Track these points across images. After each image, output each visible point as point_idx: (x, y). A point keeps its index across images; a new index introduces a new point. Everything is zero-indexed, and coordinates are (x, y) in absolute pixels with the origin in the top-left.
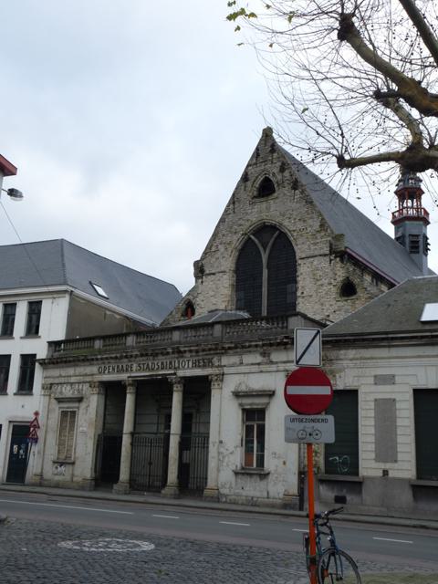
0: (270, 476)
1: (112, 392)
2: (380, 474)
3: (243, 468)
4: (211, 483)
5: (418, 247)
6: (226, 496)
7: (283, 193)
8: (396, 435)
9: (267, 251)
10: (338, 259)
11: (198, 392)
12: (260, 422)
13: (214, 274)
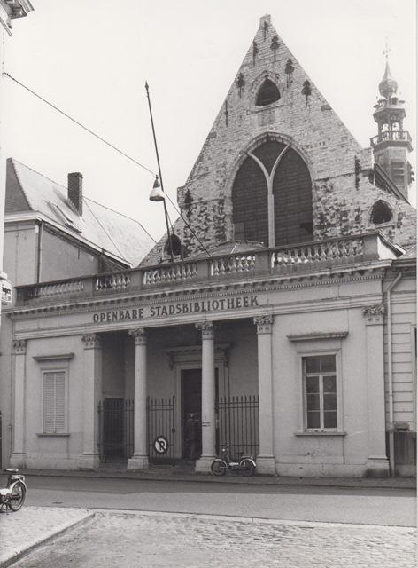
1: (114, 348)
7: (291, 97)
9: (273, 172)
10: (367, 178)
11: (237, 339)
12: (331, 374)
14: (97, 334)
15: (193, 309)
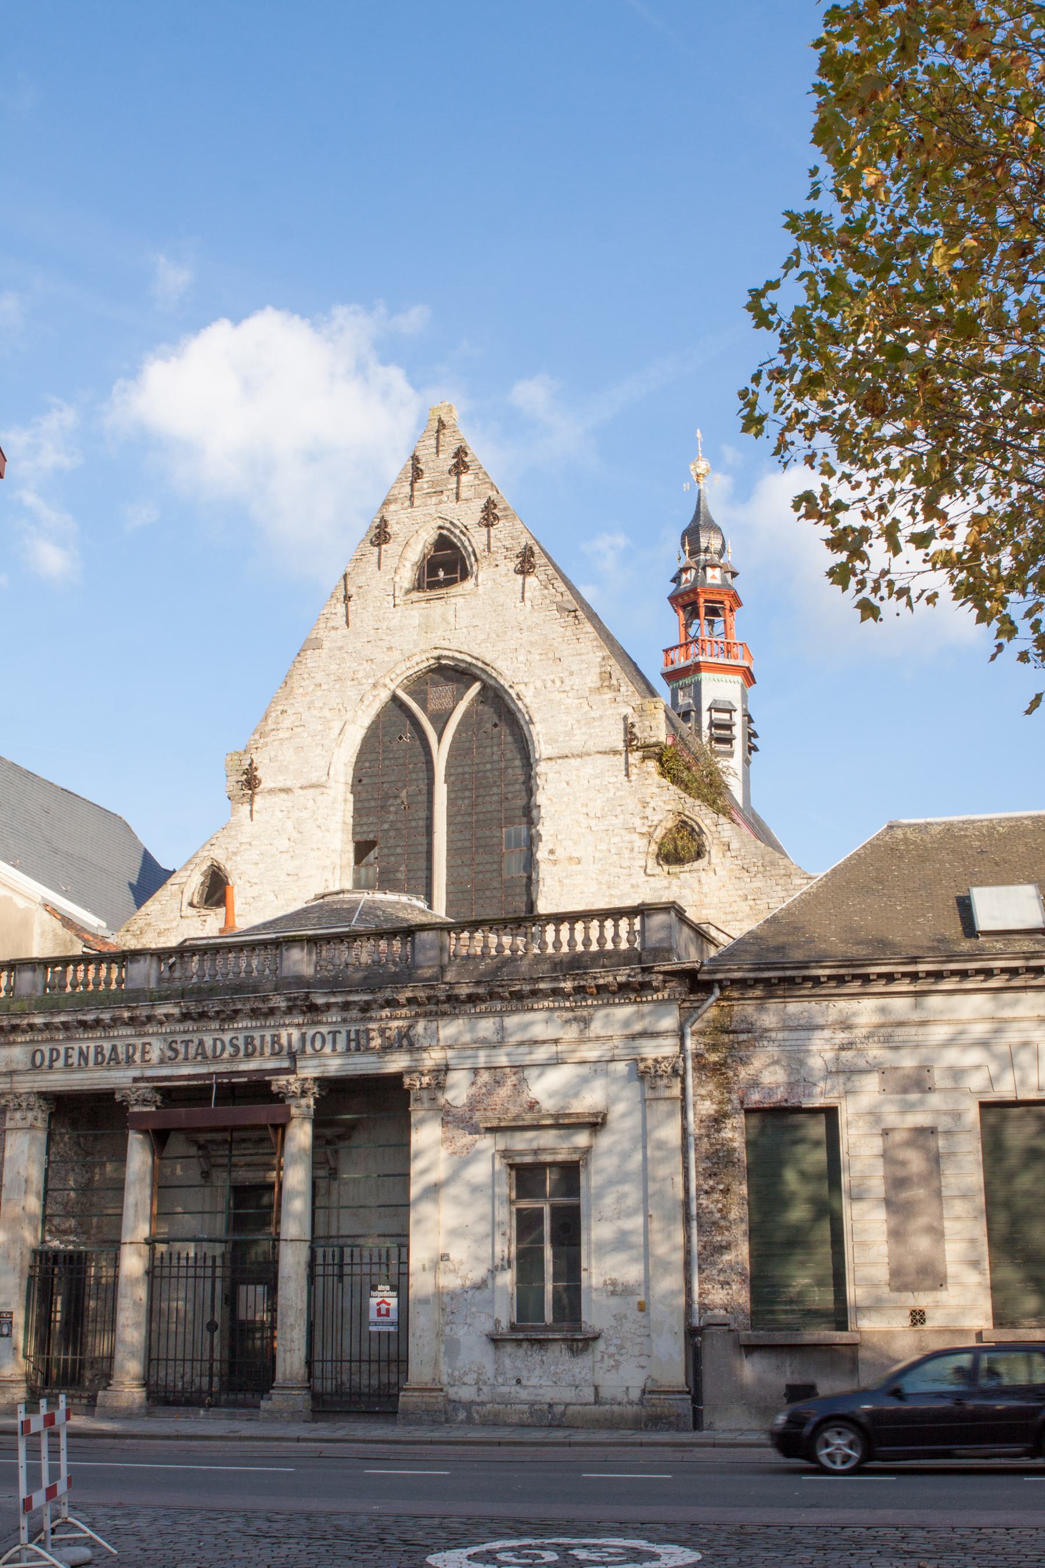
0: (601, 1345)
3: (513, 1328)
4: (419, 1371)
6: (468, 1405)
7: (492, 580)
11: (368, 1111)
12: (525, 1204)
13: (287, 790)
14: (43, 1095)
15: (268, 1051)
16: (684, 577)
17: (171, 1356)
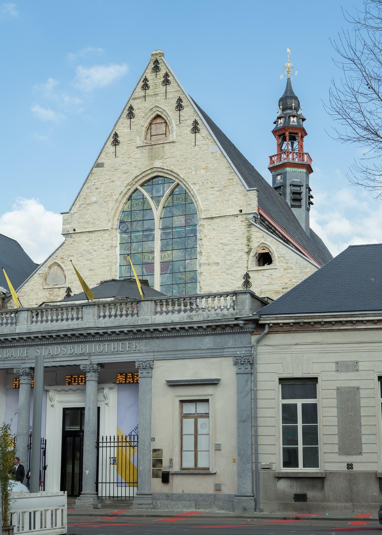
2: (343, 468)
5: (300, 200)
8: (361, 425)
9: (161, 207)
16: (280, 121)
17: (108, 484)
